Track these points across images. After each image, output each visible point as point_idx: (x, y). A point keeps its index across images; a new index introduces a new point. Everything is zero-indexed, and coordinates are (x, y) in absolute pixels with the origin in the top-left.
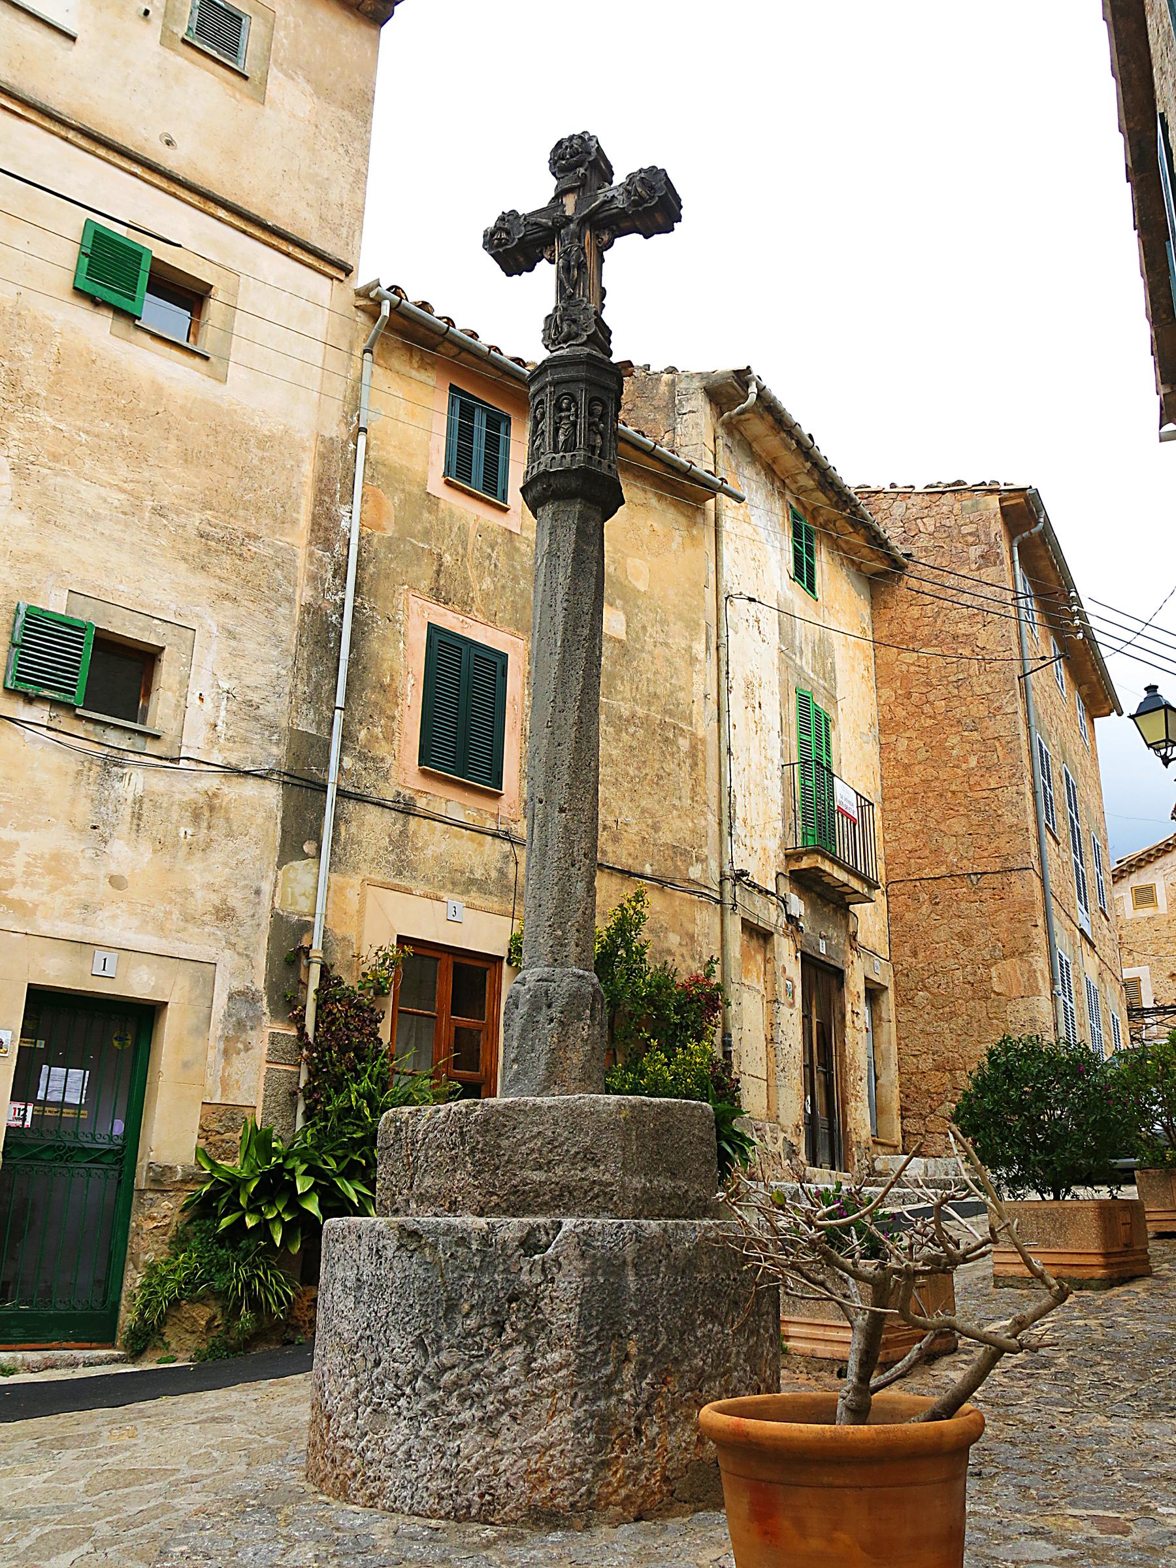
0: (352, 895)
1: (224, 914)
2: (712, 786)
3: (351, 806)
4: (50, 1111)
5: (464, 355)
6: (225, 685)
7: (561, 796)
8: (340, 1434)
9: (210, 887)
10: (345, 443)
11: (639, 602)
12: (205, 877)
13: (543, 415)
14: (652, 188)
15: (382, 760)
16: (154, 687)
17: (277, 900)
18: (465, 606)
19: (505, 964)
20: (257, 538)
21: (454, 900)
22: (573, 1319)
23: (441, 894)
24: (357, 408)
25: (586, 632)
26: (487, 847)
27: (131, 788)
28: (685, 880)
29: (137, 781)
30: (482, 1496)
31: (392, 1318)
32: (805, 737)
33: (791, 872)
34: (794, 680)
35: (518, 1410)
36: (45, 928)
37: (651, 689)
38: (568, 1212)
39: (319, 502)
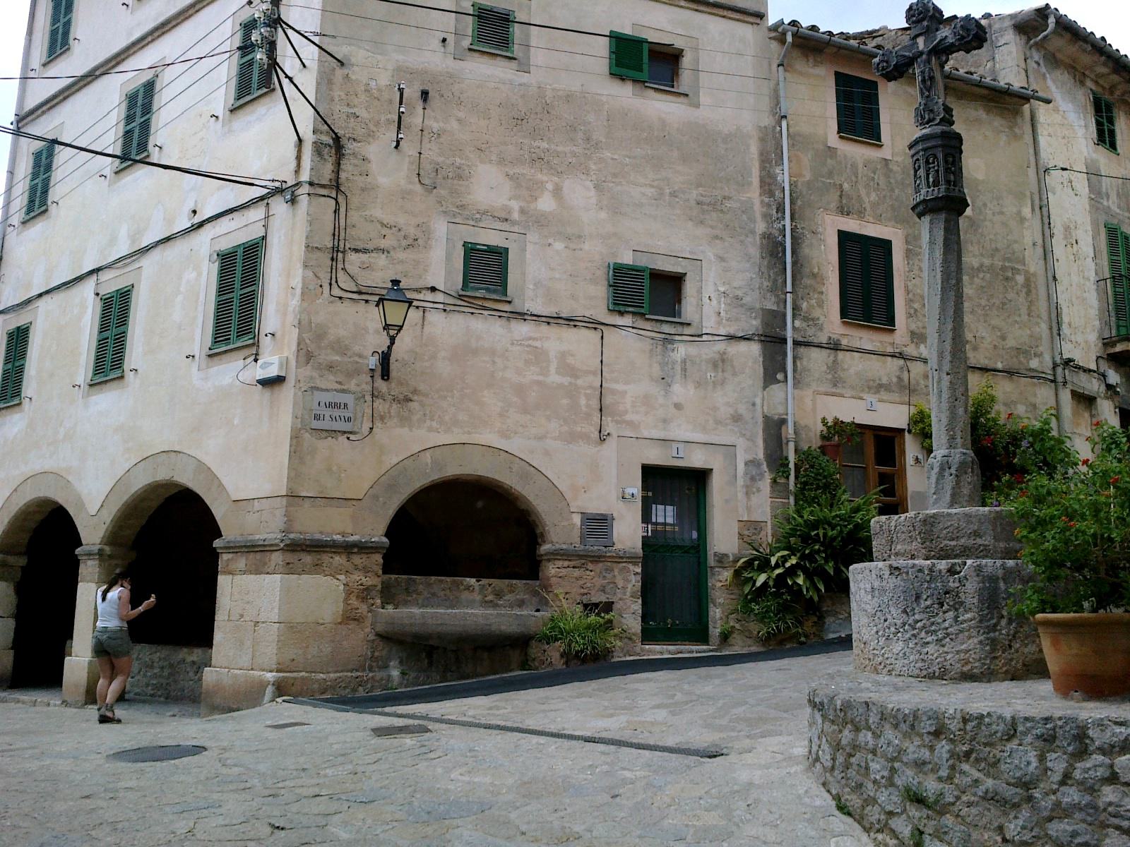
0: (808, 402)
1: (737, 418)
2: (1042, 305)
3: (802, 350)
4: (659, 528)
5: (842, 51)
6: (722, 289)
7: (947, 367)
8: (871, 648)
9: (728, 404)
10: (774, 127)
11: (980, 188)
12: (725, 399)
13: (919, 167)
14: (968, 30)
15: (818, 319)
16: (683, 296)
17: (765, 408)
18: (861, 214)
19: (906, 433)
20: (729, 198)
21: (870, 397)
22: (975, 601)
23: (861, 395)
24: (778, 103)
25: (954, 282)
26: (888, 363)
27: (679, 355)
28: (1027, 370)
29: (681, 351)
30: (940, 669)
31: (890, 602)
32: (1115, 258)
33: (1108, 355)
34: (1103, 218)
35: (954, 637)
36: (646, 434)
37: (993, 246)
38: (968, 557)
39: (762, 168)
